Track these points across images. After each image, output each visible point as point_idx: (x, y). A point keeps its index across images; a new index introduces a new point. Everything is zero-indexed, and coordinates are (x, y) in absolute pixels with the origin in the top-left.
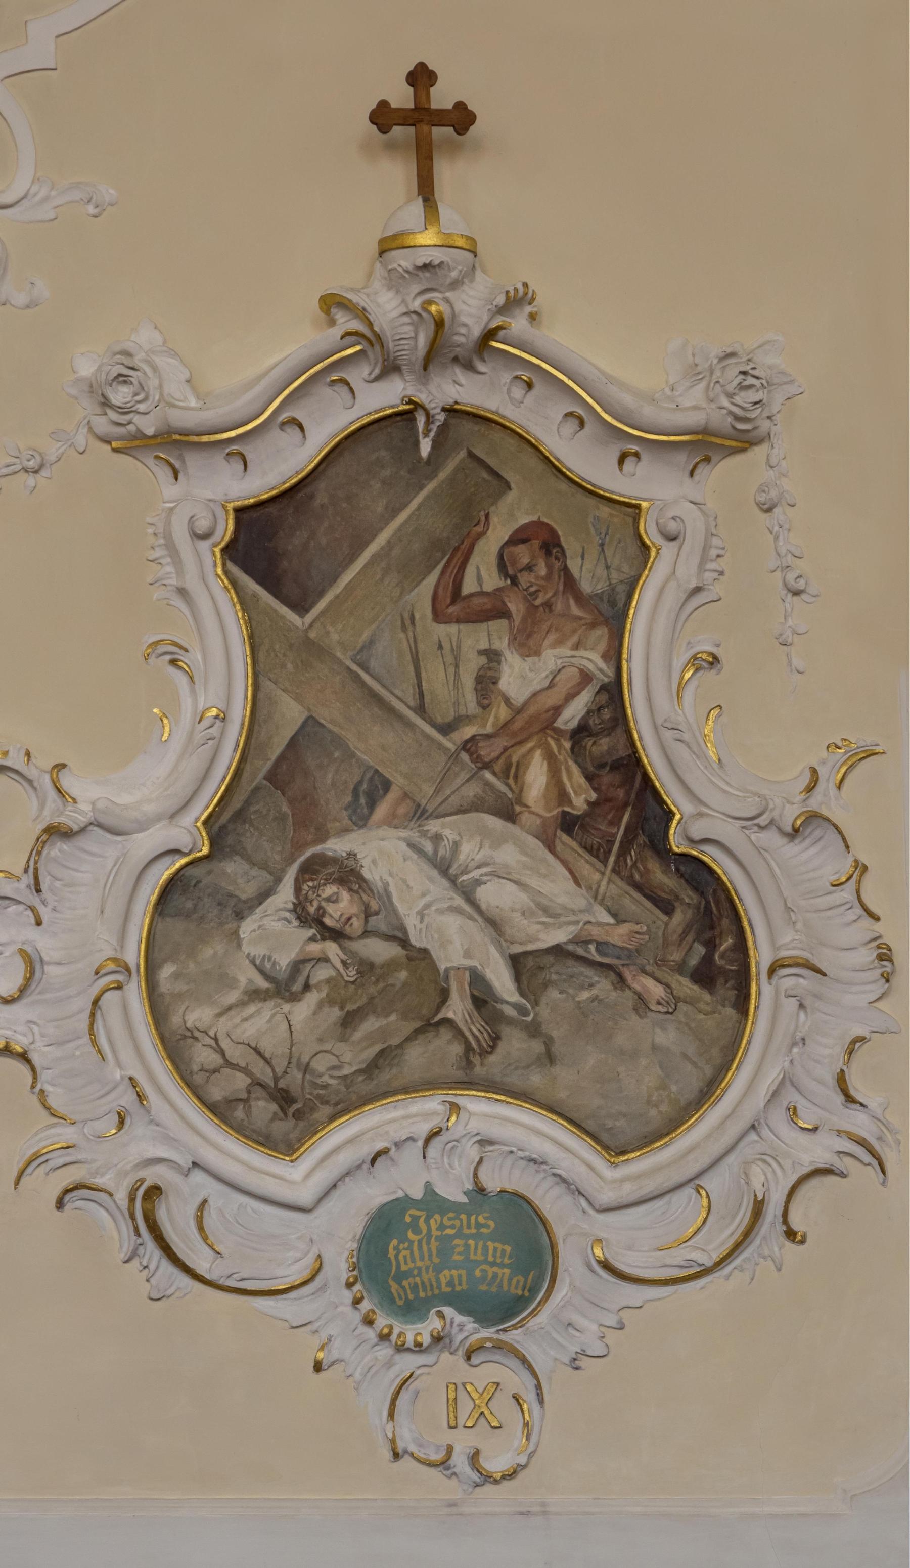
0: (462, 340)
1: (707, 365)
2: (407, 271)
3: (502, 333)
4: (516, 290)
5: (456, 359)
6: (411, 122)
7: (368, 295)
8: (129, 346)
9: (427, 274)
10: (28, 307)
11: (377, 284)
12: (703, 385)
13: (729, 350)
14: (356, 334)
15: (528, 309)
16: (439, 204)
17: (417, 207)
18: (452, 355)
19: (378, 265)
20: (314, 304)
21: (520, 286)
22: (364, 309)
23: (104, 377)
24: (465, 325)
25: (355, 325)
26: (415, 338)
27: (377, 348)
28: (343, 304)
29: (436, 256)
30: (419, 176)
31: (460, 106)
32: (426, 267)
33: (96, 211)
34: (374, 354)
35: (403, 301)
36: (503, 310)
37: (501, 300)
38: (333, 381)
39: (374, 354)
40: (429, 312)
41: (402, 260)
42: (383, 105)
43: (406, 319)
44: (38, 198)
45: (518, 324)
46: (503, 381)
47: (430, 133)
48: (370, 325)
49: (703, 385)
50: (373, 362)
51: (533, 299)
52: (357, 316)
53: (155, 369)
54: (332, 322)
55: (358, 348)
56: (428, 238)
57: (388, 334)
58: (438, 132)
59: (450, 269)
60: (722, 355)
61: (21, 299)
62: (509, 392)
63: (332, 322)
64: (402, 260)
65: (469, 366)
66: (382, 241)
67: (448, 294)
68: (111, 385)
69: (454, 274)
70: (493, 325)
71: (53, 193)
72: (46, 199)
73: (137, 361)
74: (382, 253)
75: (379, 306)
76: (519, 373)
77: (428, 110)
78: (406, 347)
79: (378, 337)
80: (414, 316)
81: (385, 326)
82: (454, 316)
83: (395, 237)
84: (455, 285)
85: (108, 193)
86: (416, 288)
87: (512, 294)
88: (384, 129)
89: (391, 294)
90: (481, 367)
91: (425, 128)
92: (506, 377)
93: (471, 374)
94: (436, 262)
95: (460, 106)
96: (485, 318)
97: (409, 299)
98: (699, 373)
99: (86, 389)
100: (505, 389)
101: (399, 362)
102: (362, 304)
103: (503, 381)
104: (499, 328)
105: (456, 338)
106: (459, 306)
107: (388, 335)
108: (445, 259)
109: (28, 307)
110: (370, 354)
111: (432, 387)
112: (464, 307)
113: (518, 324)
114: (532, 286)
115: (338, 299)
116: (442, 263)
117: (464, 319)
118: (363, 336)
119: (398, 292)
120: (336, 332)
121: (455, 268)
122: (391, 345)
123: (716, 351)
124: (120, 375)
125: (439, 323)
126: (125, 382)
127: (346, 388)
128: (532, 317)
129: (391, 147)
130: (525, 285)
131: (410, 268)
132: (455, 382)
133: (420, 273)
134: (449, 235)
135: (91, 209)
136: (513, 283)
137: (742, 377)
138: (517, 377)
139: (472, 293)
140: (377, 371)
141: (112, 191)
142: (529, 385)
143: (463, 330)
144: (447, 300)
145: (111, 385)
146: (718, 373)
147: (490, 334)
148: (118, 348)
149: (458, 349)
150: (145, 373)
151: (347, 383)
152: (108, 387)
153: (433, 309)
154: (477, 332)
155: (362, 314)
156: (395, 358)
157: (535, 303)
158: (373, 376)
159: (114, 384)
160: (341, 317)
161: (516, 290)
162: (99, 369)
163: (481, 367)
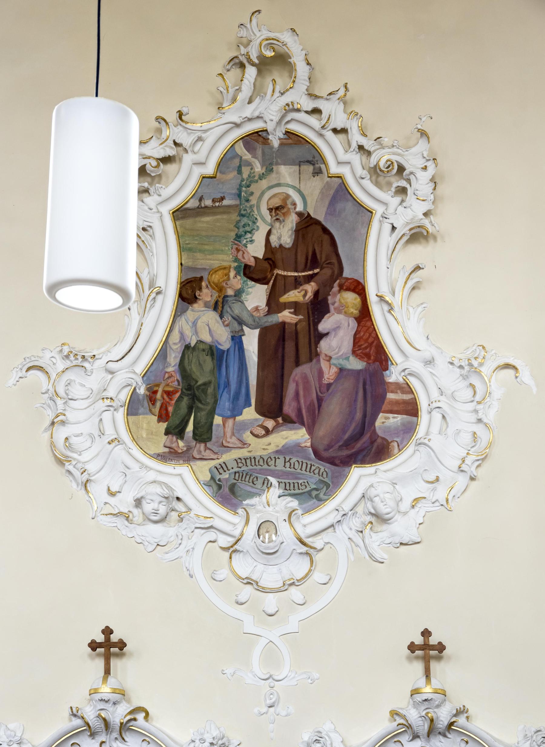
0: (441, 726)
1: (531, 735)
2: (420, 702)
3: (455, 724)
4: (460, 708)
5: (440, 733)
6: (422, 649)
7: (407, 710)
8: (320, 729)
9: (427, 703)
10: (286, 716)
11: (410, 707)
12: (529, 742)
13: (538, 729)
14: (402, 724)
15: (466, 715)
16: (431, 678)
17: (424, 679)
18: (438, 732)
19: (411, 700)
20: (388, 715)
21: (462, 707)
22: (405, 715)
23: (311, 741)
24: (442, 721)
25: (402, 721)
26: (424, 726)
27: (410, 729)
28: (397, 714)
29: (429, 696)
30: (425, 668)
31: (440, 643)
32: (426, 700)
33: (312, 682)
34: (409, 731)
35: (419, 713)
36: (455, 715)
37: (454, 712)
38: (395, 741)
39: (409, 731)
40: (428, 716)
41: (419, 698)
42: (412, 643)
43: (420, 719)
44: (291, 677)
45: (461, 720)
46: (458, 741)
47: (429, 652)
48: (407, 721)
49: (529, 742)
50: (409, 734)
51: (467, 711)
52: (403, 718)
53: (329, 737)
54: (395, 720)
55: (404, 729)
56: (428, 689)
57: (414, 724)
58: (432, 653)
59: (435, 701)
60: (536, 731)
61: (284, 713)
62: (460, 744)
63: (395, 720)
64: (419, 698)
65: (445, 736)
66: (411, 691)
67: (435, 710)
68: (313, 743)
69: (437, 703)
70: (452, 721)
71: (296, 675)
72: (294, 678)
73: (323, 735)
74: (411, 695)
75: (410, 714)
76: (463, 738)
77: (428, 645)
78: (421, 729)
79: (410, 725)
80: (423, 718)
81: (413, 722)
82: (438, 718)
83: (416, 690)
84: (438, 706)
85: (316, 675)
86: (423, 708)
87: (459, 709)
88: (94, 649)
89: (415, 710)
90: (449, 736)
91: (427, 651)
92: (459, 739)
93: (446, 738)
94: (429, 699)
95: (103, 632)
96: (449, 718)
97: (421, 712)
98: (527, 738)
99: (306, 745)
100: (458, 744)
101: (419, 734)
102: (404, 713)
103: (458, 741)
104: (454, 722)
105: (439, 725)
106: (439, 714)
107: (414, 725)
108: (433, 697)
109: (286, 716)
110: (408, 731)
111: (431, 743)
112: (442, 715)
113: (461, 720)
114: (467, 707)
115: (395, 712)
116: (432, 699)
117: (441, 719)
118: (405, 725)
119: (417, 709)
120: (396, 724)
121: (437, 701)
122: (415, 728)
123: (534, 730)
124: (316, 740)
125: (432, 720)
126: (319, 742)
127: (400, 744)
128: (467, 718)
129: (417, 658)
130: (464, 706)
131: (421, 701)
132: (440, 741)
133: (424, 703)
134: (435, 689)
135: (310, 681)
136: (459, 706)
137: (543, 739)
138: (462, 740)
139: (445, 709)
140: (411, 738)
141: (317, 674)
142: (467, 742)
143: (441, 723)
144: (435, 712)
145: (313, 743)
146: (534, 737)
147: (452, 724)
148: (316, 730)
149: (440, 730)
150: (326, 739)
151: (401, 742)
152: (312, 744)
153: (429, 715)
154: (446, 723)
155: (404, 717)
156: (417, 733)
157: (468, 713)
158: (410, 739)
159: (315, 743)
160: (397, 718)
161: (460, 708)
162: (309, 738)
163: (449, 736)
